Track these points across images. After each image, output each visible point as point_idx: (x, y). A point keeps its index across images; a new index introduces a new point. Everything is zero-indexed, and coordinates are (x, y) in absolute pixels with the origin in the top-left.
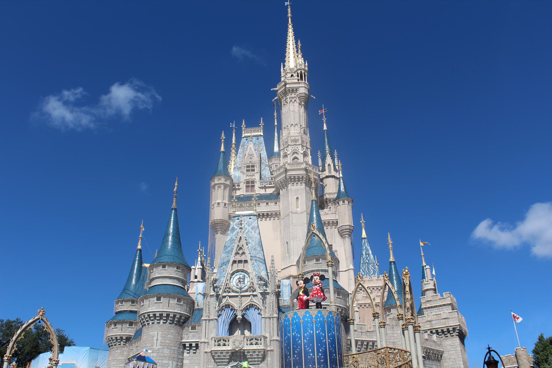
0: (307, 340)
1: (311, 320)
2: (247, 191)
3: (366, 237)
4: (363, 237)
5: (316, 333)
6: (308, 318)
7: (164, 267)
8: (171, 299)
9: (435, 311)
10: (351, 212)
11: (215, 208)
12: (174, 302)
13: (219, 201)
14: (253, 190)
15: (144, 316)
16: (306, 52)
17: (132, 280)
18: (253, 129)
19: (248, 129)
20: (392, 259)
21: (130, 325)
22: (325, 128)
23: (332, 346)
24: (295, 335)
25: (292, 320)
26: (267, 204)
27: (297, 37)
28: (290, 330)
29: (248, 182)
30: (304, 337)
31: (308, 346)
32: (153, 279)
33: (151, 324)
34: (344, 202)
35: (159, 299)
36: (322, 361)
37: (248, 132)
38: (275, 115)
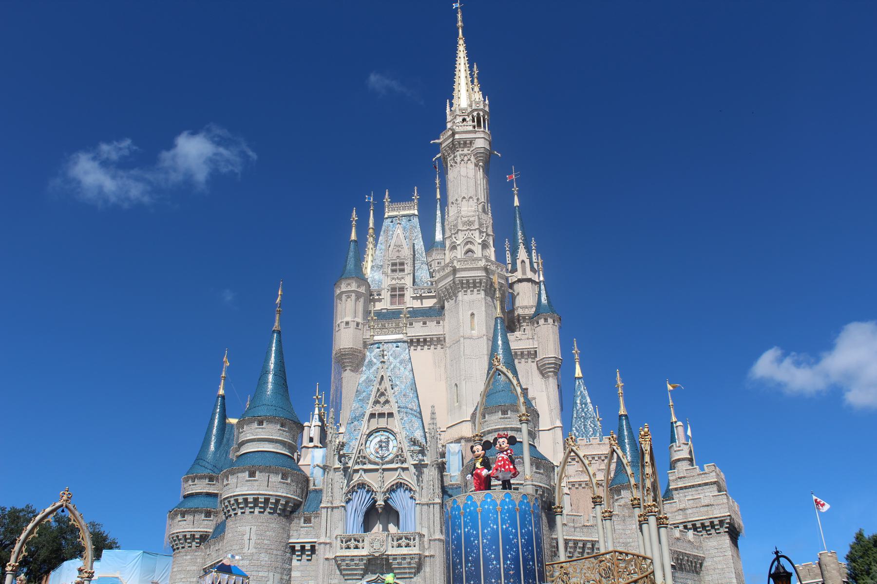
0: (487, 539)
1: (494, 508)
2: (392, 304)
3: (581, 375)
4: (577, 375)
5: (502, 528)
6: (489, 504)
7: (261, 423)
8: (271, 475)
9: (691, 494)
10: (557, 337)
11: (342, 330)
12: (276, 479)
13: (348, 319)
14: (401, 302)
15: (229, 502)
16: (486, 82)
17: (210, 444)
18: (403, 204)
19: (395, 205)
20: (622, 411)
21: (206, 516)
22: (516, 203)
23: (527, 550)
24: (469, 531)
25: (464, 509)
26: (425, 323)
27: (471, 59)
28: (460, 523)
29: (393, 289)
30: (484, 535)
31: (490, 550)
32: (243, 443)
33: (239, 514)
34: (546, 320)
35: (252, 474)
36: (511, 572)
37: (393, 210)
38: (437, 182)
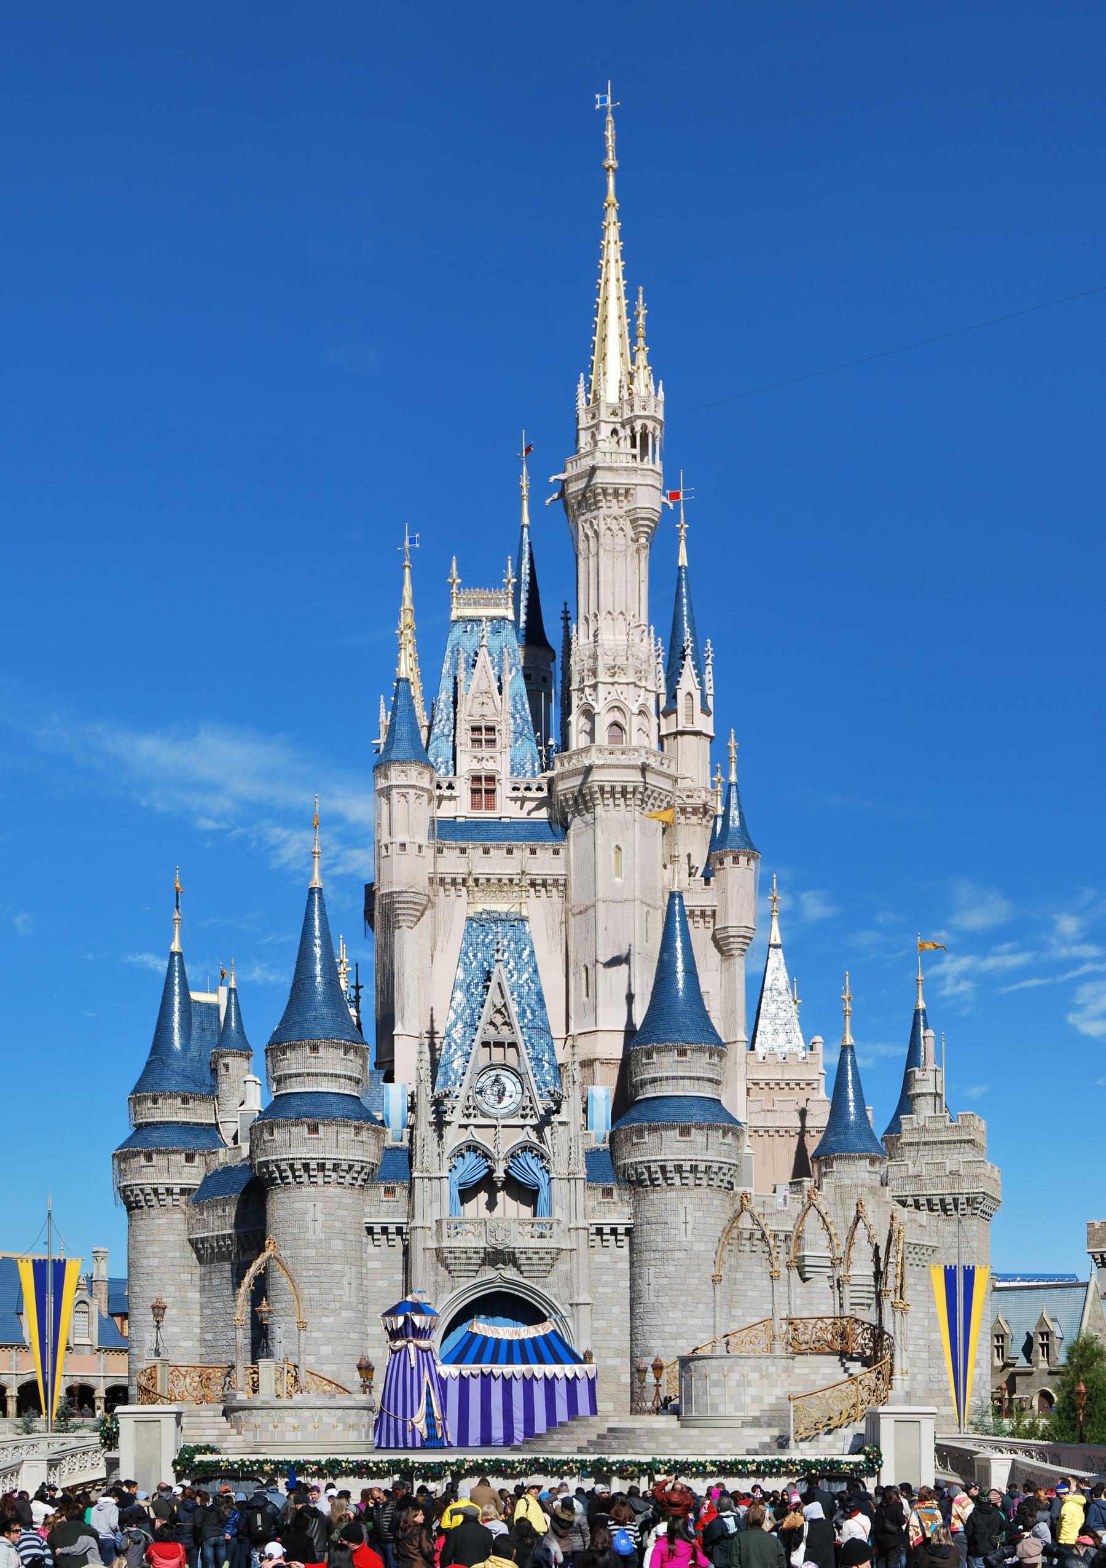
2: (475, 805)
3: (779, 941)
4: (772, 942)
7: (685, 1131)
8: (341, 1129)
9: (926, 1156)
10: (793, 1163)
11: (395, 858)
12: (347, 1134)
13: (400, 838)
14: (491, 806)
15: (132, 1191)
16: (665, 348)
17: (171, 1038)
18: (486, 594)
19: (466, 594)
20: (175, 947)
21: (681, 1134)
22: (683, 560)
26: (533, 852)
27: (529, 473)
29: (476, 779)
32: (643, 1084)
33: (77, 1468)
34: (736, 860)
35: (314, 1129)
36: (814, 1471)
37: (467, 604)
38: (524, 483)
